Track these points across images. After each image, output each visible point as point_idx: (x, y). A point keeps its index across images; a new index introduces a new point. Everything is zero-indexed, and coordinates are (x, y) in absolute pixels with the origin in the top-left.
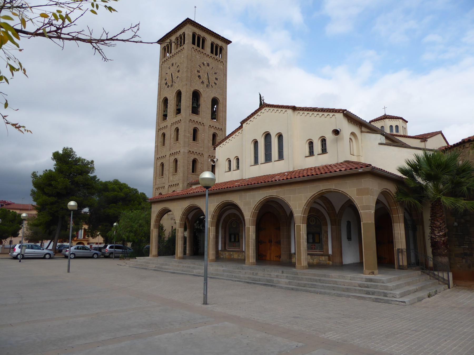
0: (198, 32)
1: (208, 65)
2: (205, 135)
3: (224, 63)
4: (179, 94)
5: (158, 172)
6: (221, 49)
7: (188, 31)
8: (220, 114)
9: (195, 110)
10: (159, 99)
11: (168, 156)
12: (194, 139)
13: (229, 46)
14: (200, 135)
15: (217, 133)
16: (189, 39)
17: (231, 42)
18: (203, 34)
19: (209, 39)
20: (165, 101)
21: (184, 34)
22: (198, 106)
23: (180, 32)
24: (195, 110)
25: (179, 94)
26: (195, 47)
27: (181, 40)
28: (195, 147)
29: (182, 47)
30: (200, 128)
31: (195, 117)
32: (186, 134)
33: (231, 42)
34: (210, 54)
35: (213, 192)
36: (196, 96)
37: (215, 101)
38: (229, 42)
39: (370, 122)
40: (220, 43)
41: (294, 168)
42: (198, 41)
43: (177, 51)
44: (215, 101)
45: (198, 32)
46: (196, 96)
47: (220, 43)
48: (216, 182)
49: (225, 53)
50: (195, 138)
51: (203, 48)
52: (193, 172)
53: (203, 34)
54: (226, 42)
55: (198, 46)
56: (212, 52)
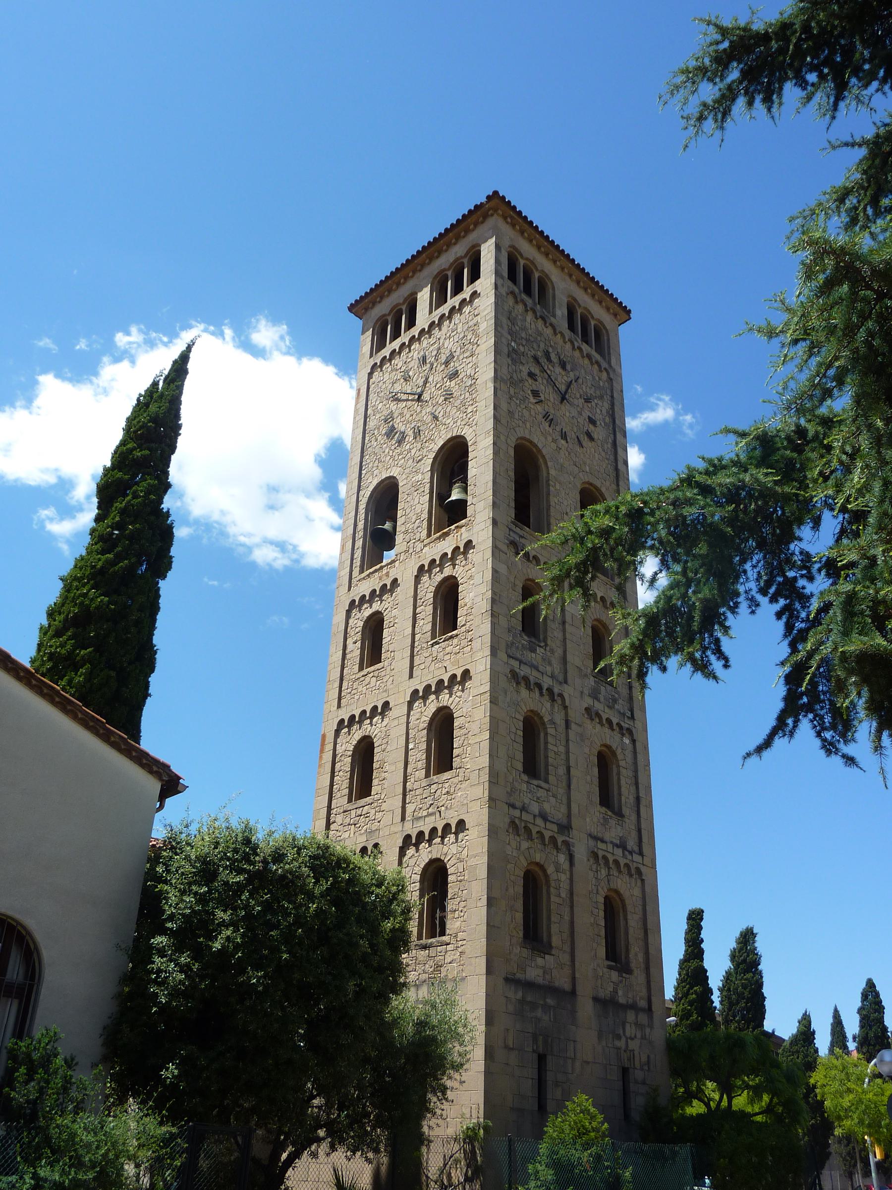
9: (451, 513)
38: (623, 313)
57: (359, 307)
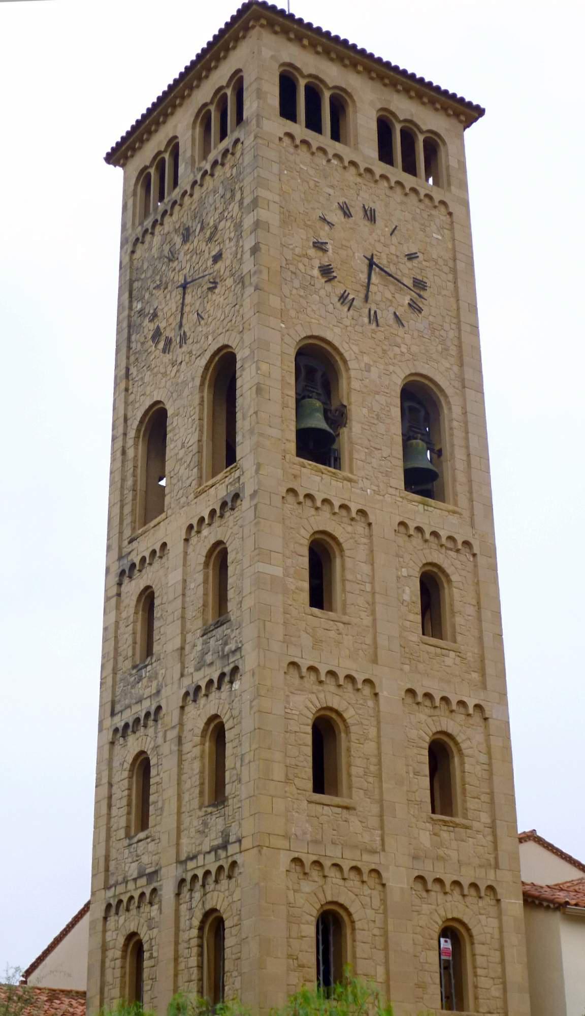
0: (309, 63)
1: (370, 216)
2: (376, 577)
3: (453, 215)
4: (223, 373)
6: (433, 147)
7: (262, 59)
9: (318, 446)
10: (121, 421)
11: (171, 715)
12: (319, 596)
15: (445, 565)
16: (262, 99)
17: (479, 112)
18: (333, 74)
19: (367, 103)
24: (318, 446)
25: (223, 373)
26: (299, 129)
28: (332, 642)
29: (227, 142)
31: (314, 478)
32: (270, 566)
33: (479, 112)
36: (317, 369)
37: (421, 406)
38: (469, 113)
39: (531, 837)
40: (430, 120)
41: (91, 998)
42: (311, 105)
45: (309, 63)
46: (317, 369)
47: (430, 120)
48: (519, 832)
49: (453, 163)
50: (324, 776)
52: (319, 786)
53: (333, 74)
54: (457, 115)
55: (314, 124)
56: (386, 155)
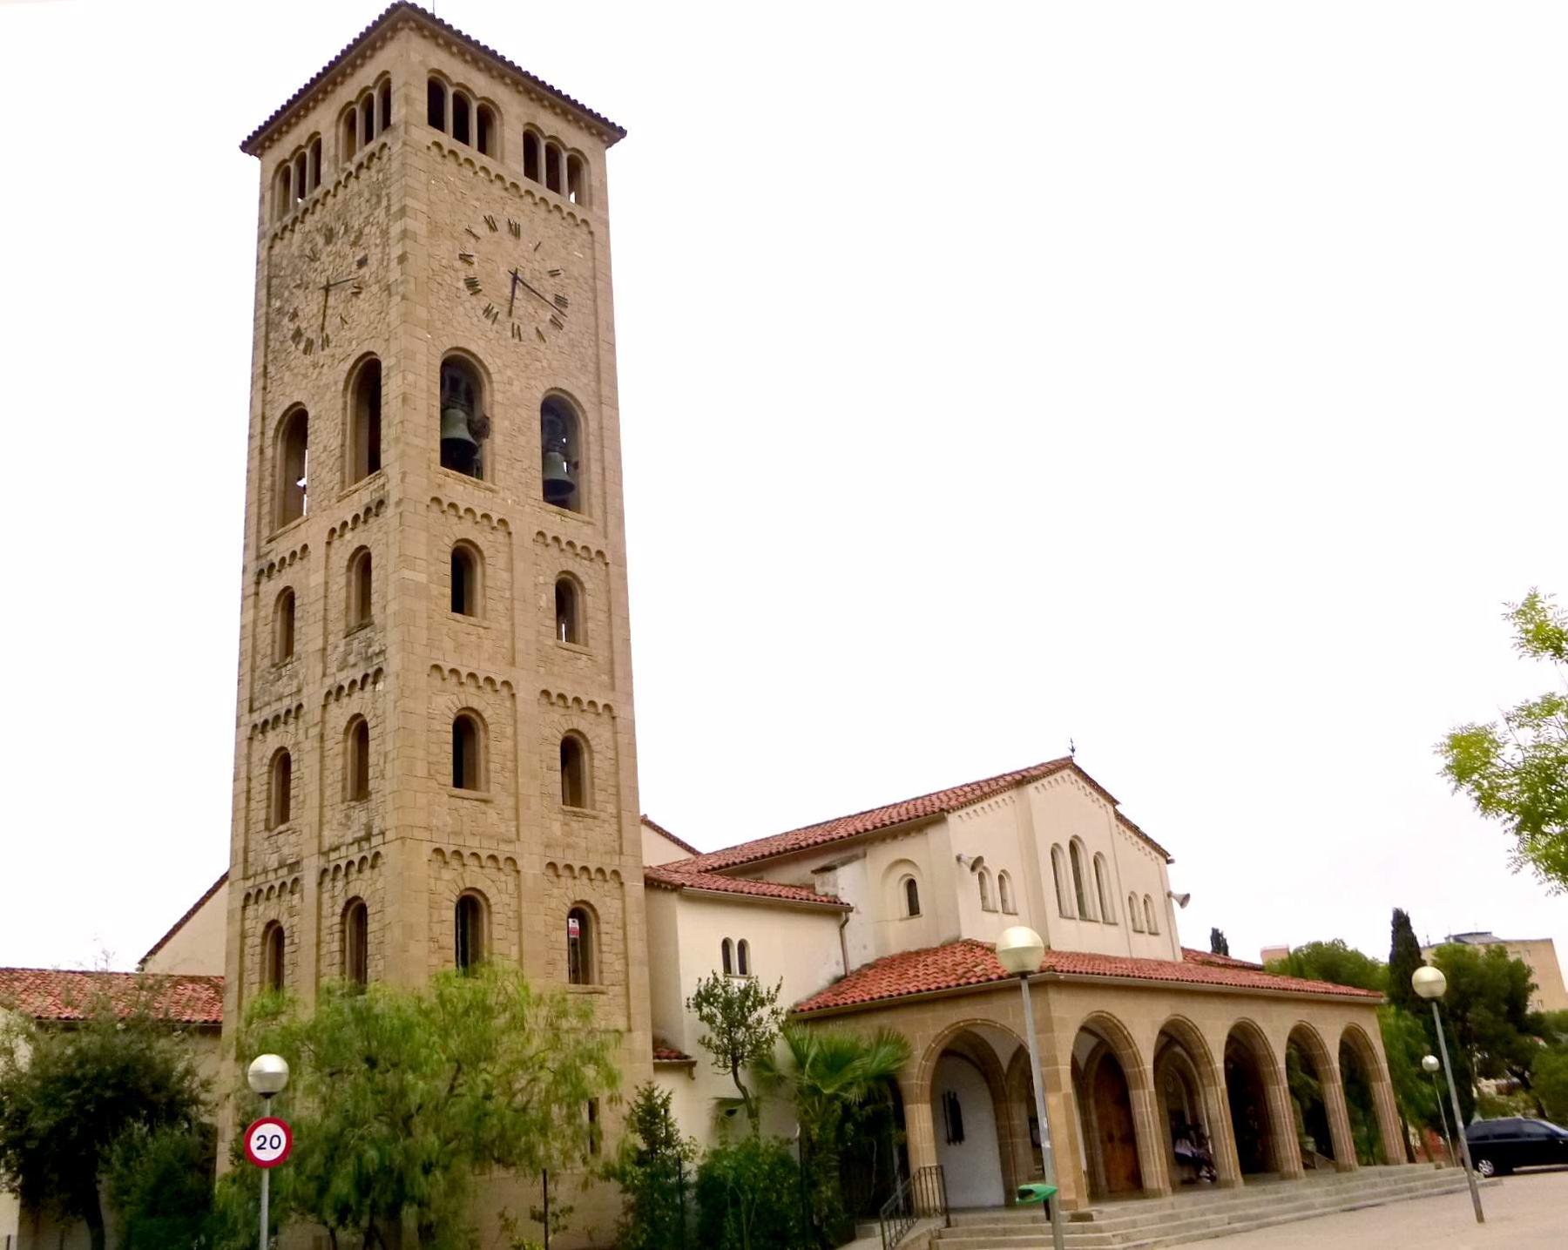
3: (591, 232)
5: (259, 813)
6: (576, 166)
8: (590, 484)
9: (461, 456)
10: (259, 418)
12: (461, 600)
13: (615, 154)
14: (490, 579)
16: (410, 105)
17: (622, 133)
19: (514, 117)
20: (295, 427)
21: (316, 143)
22: (481, 428)
23: (366, 76)
24: (461, 456)
26: (447, 139)
27: (370, 117)
28: (474, 645)
30: (497, 892)
31: (457, 487)
32: (412, 572)
33: (622, 133)
34: (525, 183)
35: (506, 309)
36: (460, 380)
37: (559, 418)
38: (610, 133)
40: (574, 139)
43: (360, 156)
44: (559, 418)
45: (458, 72)
46: (460, 380)
49: (595, 183)
51: (482, 148)
52: (458, 782)
53: (481, 85)
54: (600, 134)
55: (461, 134)
56: (531, 171)
57: (255, 144)
